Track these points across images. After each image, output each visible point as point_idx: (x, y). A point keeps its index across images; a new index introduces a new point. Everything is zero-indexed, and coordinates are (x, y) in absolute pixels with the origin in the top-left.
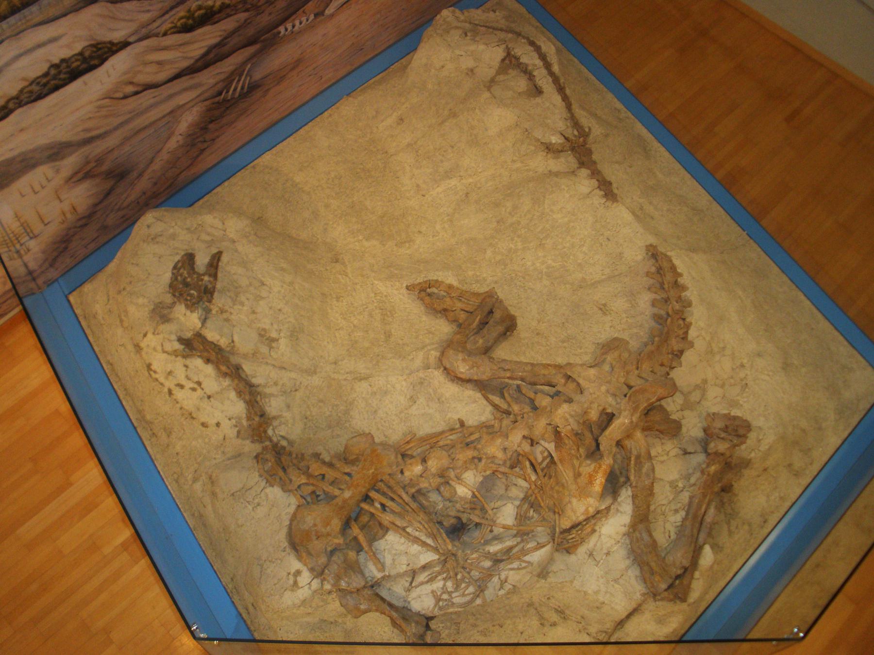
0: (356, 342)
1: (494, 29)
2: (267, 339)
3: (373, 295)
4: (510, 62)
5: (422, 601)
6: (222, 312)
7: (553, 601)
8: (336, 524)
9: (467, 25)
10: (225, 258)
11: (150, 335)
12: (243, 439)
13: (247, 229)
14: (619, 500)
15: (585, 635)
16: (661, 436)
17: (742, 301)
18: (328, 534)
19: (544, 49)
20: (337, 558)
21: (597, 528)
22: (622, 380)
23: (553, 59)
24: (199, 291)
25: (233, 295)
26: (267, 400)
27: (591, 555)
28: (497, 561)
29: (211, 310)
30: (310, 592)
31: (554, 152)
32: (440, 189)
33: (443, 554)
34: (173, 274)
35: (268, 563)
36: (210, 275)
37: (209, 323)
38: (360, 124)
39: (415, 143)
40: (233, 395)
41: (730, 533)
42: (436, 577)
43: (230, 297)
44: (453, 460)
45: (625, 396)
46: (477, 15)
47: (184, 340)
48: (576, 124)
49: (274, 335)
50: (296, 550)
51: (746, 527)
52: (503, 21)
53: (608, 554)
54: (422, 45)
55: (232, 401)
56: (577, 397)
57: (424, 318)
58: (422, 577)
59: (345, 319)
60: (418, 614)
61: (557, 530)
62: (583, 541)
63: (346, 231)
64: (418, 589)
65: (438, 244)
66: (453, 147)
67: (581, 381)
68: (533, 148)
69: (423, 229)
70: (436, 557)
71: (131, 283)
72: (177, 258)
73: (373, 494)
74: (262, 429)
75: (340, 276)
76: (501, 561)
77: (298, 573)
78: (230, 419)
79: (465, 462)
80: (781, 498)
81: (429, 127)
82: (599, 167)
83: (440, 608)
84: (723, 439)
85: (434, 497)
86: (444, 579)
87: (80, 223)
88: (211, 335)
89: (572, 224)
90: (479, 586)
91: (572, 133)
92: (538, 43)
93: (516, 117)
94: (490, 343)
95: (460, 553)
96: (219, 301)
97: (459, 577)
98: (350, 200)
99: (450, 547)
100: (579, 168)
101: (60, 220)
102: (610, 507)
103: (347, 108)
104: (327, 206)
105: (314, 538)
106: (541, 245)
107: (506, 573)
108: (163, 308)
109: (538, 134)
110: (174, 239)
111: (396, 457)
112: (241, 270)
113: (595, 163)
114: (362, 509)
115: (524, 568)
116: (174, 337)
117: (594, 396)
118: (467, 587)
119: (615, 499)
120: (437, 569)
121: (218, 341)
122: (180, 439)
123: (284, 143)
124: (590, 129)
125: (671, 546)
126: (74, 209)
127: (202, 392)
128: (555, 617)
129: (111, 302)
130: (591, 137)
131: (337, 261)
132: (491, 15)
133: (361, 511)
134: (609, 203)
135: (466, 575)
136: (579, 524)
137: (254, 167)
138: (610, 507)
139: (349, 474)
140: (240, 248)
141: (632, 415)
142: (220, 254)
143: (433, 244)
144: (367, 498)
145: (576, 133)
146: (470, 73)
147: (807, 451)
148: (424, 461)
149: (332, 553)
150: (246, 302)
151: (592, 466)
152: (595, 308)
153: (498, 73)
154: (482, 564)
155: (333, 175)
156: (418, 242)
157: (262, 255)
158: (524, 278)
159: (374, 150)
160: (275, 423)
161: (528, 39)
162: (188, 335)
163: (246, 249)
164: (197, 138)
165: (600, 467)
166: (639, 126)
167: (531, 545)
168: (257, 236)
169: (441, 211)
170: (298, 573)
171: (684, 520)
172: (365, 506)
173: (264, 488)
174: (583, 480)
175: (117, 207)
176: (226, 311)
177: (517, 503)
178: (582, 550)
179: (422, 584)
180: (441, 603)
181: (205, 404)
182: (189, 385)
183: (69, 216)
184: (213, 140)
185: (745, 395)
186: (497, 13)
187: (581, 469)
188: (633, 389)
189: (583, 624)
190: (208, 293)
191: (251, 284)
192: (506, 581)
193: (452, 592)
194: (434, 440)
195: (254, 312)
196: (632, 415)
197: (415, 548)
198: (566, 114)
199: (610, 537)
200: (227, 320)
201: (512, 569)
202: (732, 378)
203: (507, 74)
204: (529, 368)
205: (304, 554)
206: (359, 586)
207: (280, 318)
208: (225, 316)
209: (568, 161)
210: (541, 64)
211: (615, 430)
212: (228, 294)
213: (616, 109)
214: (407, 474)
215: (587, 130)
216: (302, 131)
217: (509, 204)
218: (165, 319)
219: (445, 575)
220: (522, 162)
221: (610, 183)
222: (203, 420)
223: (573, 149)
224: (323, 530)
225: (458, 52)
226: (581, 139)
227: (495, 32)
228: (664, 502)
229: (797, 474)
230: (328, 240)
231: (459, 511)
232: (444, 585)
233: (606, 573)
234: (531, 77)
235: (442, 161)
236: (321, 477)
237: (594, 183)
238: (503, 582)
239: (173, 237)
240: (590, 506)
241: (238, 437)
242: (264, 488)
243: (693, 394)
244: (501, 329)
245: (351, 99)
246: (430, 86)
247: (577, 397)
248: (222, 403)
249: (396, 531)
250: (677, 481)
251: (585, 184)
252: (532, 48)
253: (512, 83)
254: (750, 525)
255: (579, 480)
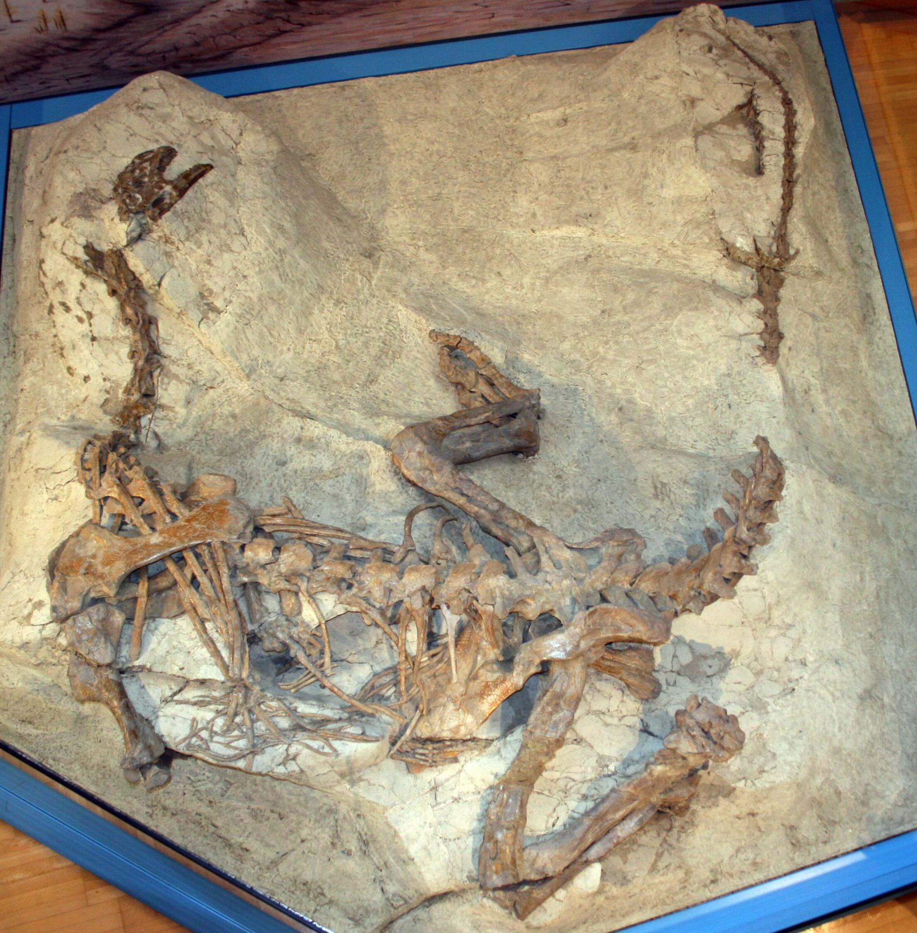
0: (325, 367)
1: (752, 60)
2: (207, 304)
3: (385, 320)
4: (747, 114)
5: (174, 725)
6: (166, 242)
7: (362, 822)
8: (120, 569)
9: (722, 39)
10: (210, 177)
11: (57, 224)
12: (105, 412)
13: (268, 157)
14: (508, 739)
15: (379, 890)
16: (627, 692)
17: (862, 580)
18: (102, 577)
19: (799, 117)
20: (97, 612)
21: (462, 759)
22: (599, 586)
23: (803, 137)
24: (146, 200)
25: (192, 227)
26: (166, 380)
27: (435, 789)
28: (298, 727)
29: (151, 231)
30: (39, 636)
31: (733, 260)
32: (558, 233)
33: (231, 679)
34: (133, 162)
35: (22, 575)
36: (175, 188)
37: (139, 247)
38: (510, 101)
39: (565, 158)
40: (125, 350)
41: (653, 869)
42: (209, 703)
43: (187, 227)
44: (315, 568)
45: (588, 608)
46: (744, 31)
47: (93, 249)
48: (782, 237)
49: (219, 303)
50: (53, 576)
51: (681, 874)
52: (772, 57)
53: (456, 800)
54: (647, 35)
55: (120, 359)
56: (523, 576)
57: (432, 382)
58: (191, 694)
59: (330, 331)
60: (159, 738)
61: (408, 732)
62: (433, 764)
63: (408, 226)
64: (179, 707)
65: (514, 301)
66: (606, 188)
67: (544, 558)
68: (707, 241)
69: (507, 272)
70: (222, 678)
71: (77, 147)
72: (154, 147)
73: (190, 557)
74: (135, 412)
75: (359, 277)
76: (304, 729)
77: (39, 605)
78: (104, 380)
79: (328, 579)
80: (755, 864)
81: (593, 147)
82: (781, 309)
83: (189, 746)
84: (693, 737)
85: (271, 603)
86: (217, 712)
87: (66, 44)
88: (135, 261)
89: (695, 362)
90: (254, 746)
91: (768, 245)
92: (796, 106)
93: (709, 190)
94: (477, 454)
95: (257, 688)
96: (166, 224)
97: (238, 719)
98: (438, 190)
99: (245, 674)
100: (754, 296)
101: (36, 24)
102: (492, 741)
103: (505, 73)
104: (404, 183)
105: (82, 571)
106: (638, 368)
107: (300, 747)
108: (93, 198)
109: (725, 225)
110: (164, 122)
111: (245, 527)
112: (222, 202)
113: (778, 299)
114: (167, 569)
115: (325, 754)
116: (82, 240)
117: (547, 586)
118: (239, 738)
119: (504, 735)
120: (216, 694)
121: (141, 275)
122: (34, 373)
123: (400, 77)
124: (797, 252)
125: (547, 837)
126: (63, 21)
127: (89, 328)
128: (353, 845)
129: (47, 161)
130: (793, 263)
131: (370, 256)
132: (764, 41)
133: (164, 572)
134: (760, 361)
135: (248, 722)
136: (441, 741)
137: (343, 88)
138: (492, 741)
139: (174, 517)
140: (241, 173)
141: (582, 637)
142: (210, 167)
143: (507, 298)
144: (179, 559)
145: (774, 249)
146: (688, 103)
147: (829, 824)
148: (278, 549)
149: (95, 601)
150: (206, 245)
151: (497, 675)
152: (650, 482)
153: (723, 121)
154: (277, 719)
155: (435, 147)
156: (489, 285)
157: (264, 198)
158: (590, 398)
159: (509, 142)
160: (159, 414)
161: (785, 94)
162: (105, 247)
163: (249, 181)
164: (278, 11)
165: (503, 681)
166: (877, 283)
167: (354, 730)
168: (275, 172)
169: (543, 261)
170: (39, 605)
171: (587, 814)
172: (171, 566)
173: (72, 480)
174: (476, 686)
175: (129, 48)
176: (173, 243)
177: (378, 669)
178: (428, 776)
179: (186, 702)
180: (194, 740)
181: (84, 346)
182: (77, 311)
183: (51, 25)
184: (303, 25)
185: (780, 701)
186: (772, 43)
187: (481, 671)
188: (604, 605)
189: (383, 873)
190: (159, 207)
191: (225, 226)
192: (294, 759)
193: (216, 733)
194: (308, 531)
195: (209, 262)
196: (582, 637)
197: (203, 653)
198: (776, 217)
199: (472, 779)
200: (168, 255)
201: (308, 747)
202: (778, 670)
203: (734, 128)
204: (494, 507)
205: (56, 584)
206: (101, 662)
207: (239, 287)
208: (169, 248)
209: (741, 279)
210: (783, 135)
211: (555, 646)
212: (186, 222)
213: (860, 246)
214: (248, 553)
215: (792, 252)
216: (432, 73)
217: (631, 296)
218: (86, 212)
219: (221, 707)
220: (684, 252)
221: (781, 336)
222: (71, 364)
223: (760, 269)
224: (100, 568)
225: (685, 68)
226: (777, 260)
227: (751, 65)
228: (577, 777)
229: (796, 845)
230: (379, 226)
231: (291, 637)
232: (213, 720)
233: (440, 823)
234: (759, 149)
235: (582, 198)
236: (138, 501)
237: (760, 325)
238: (289, 758)
239: (165, 118)
240: (465, 725)
241: (102, 406)
242: (72, 480)
243: (709, 662)
244: (507, 443)
245: (518, 62)
246: (626, 95)
247: (523, 576)
248: (106, 355)
249: (193, 619)
250: (610, 759)
251: (746, 320)
252: (782, 109)
253: (732, 143)
254: (688, 873)
255: (471, 684)
